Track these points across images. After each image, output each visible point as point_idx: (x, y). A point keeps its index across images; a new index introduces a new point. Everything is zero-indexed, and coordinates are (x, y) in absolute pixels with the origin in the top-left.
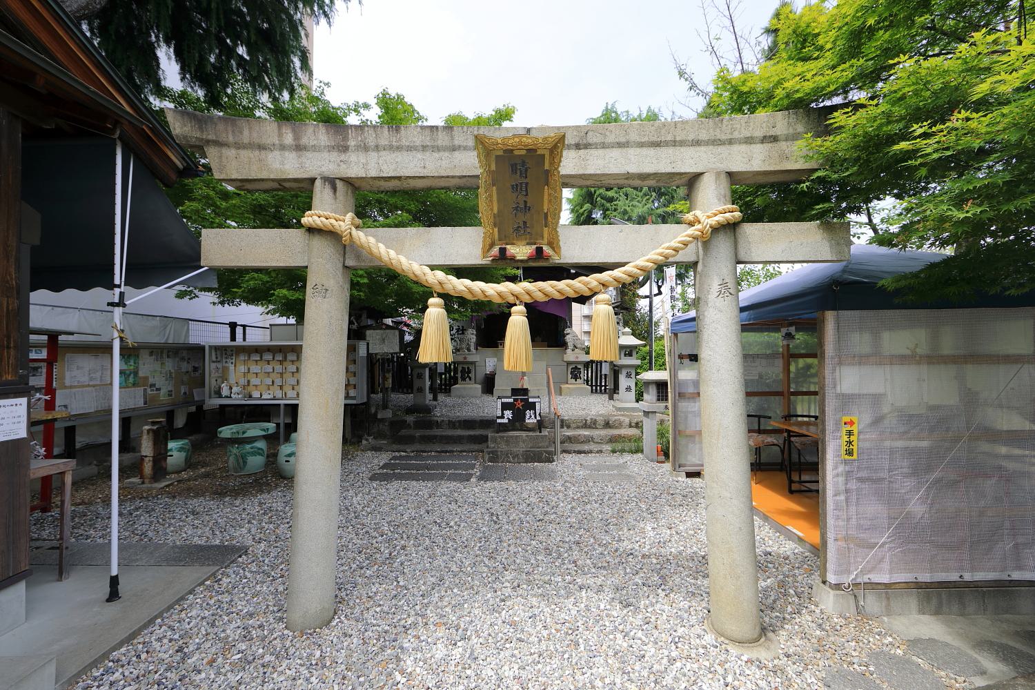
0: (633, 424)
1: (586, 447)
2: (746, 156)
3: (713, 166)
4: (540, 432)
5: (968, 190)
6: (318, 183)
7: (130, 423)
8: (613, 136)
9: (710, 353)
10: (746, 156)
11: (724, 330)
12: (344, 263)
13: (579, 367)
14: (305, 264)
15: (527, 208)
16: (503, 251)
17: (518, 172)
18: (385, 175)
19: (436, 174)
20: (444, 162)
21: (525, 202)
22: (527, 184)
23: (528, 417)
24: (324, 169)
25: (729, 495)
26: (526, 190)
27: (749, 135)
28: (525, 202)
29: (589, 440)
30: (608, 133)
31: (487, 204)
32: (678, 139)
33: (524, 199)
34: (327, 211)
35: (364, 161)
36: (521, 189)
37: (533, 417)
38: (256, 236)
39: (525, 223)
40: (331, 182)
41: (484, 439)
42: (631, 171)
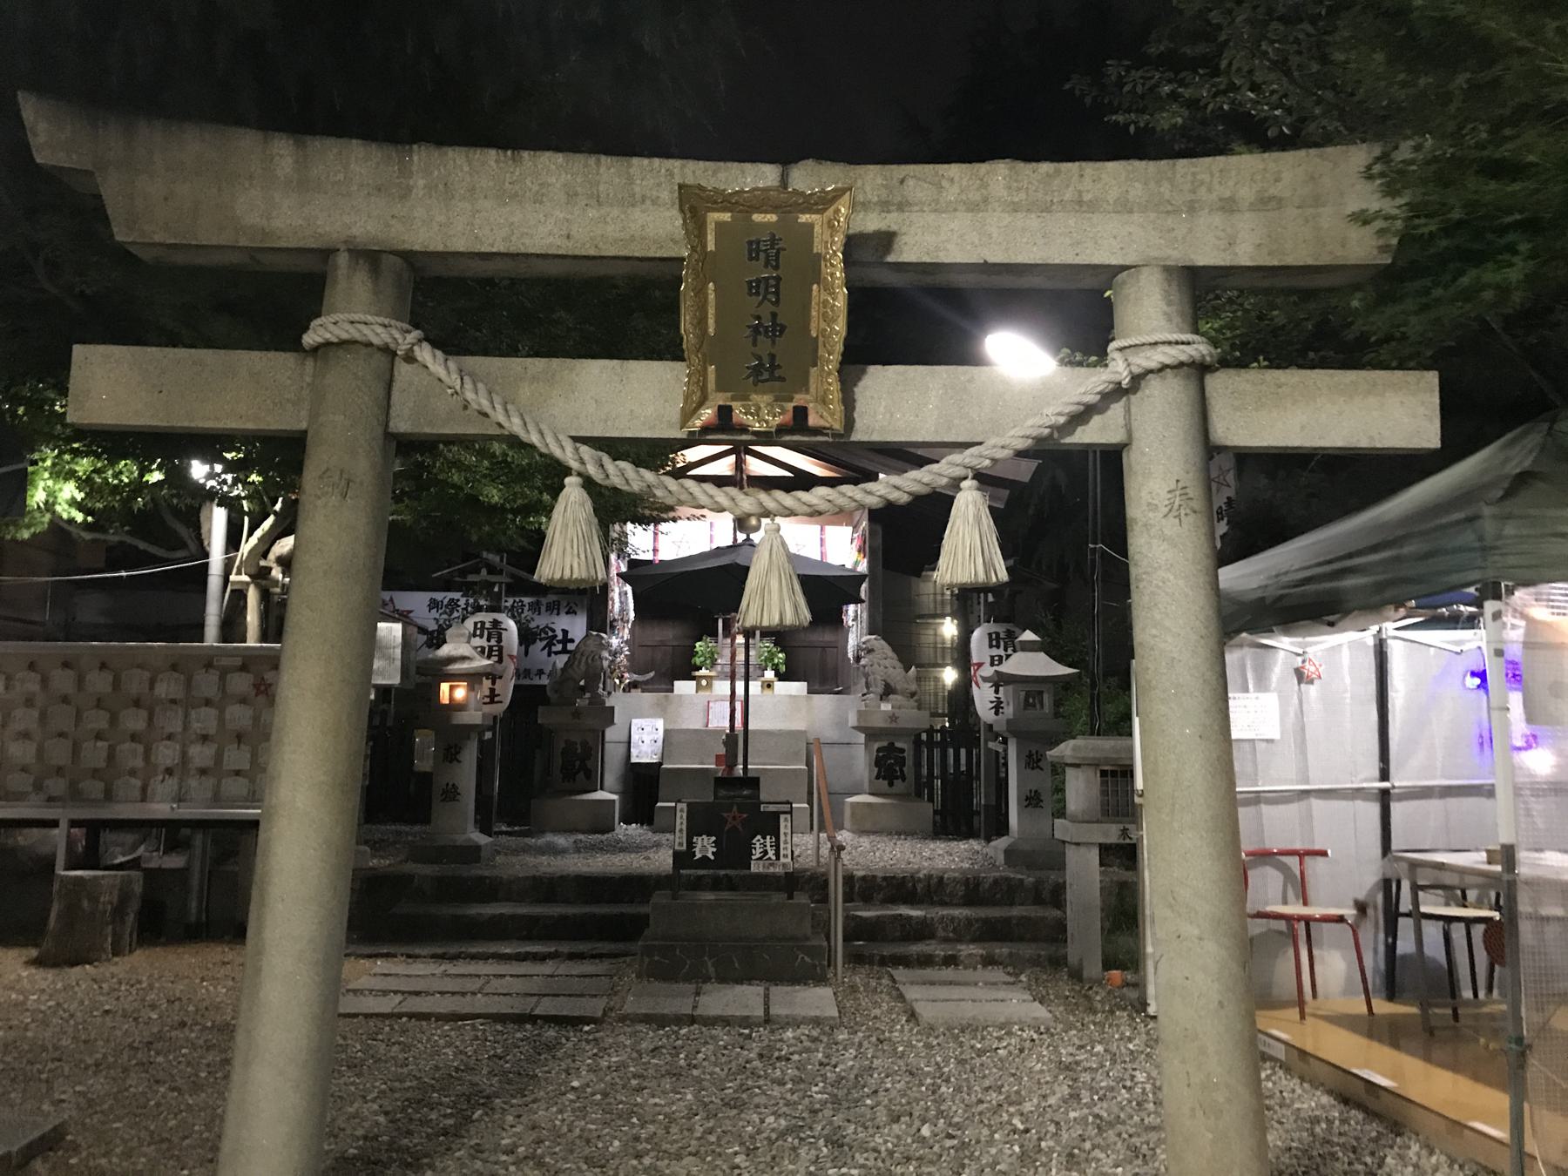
0: (1046, 894)
1: (916, 949)
2: (1222, 235)
3: (1154, 253)
4: (791, 897)
5: (82, 292)
6: (343, 259)
7: (673, 359)
8: (956, 189)
9: (1154, 632)
10: (1222, 235)
11: (1181, 583)
12: (387, 425)
13: (898, 745)
14: (304, 426)
15: (777, 329)
16: (725, 412)
17: (762, 255)
18: (485, 249)
19: (592, 252)
20: (609, 229)
21: (774, 315)
22: (778, 279)
23: (757, 854)
24: (355, 231)
25: (1196, 932)
26: (777, 293)
27: (1228, 194)
28: (774, 315)
29: (922, 931)
30: (945, 183)
31: (701, 311)
32: (1087, 197)
33: (774, 309)
34: (353, 316)
35: (442, 219)
36: (767, 292)
37: (771, 854)
38: (194, 363)
39: (772, 357)
40: (370, 257)
41: (640, 923)
42: (992, 259)
